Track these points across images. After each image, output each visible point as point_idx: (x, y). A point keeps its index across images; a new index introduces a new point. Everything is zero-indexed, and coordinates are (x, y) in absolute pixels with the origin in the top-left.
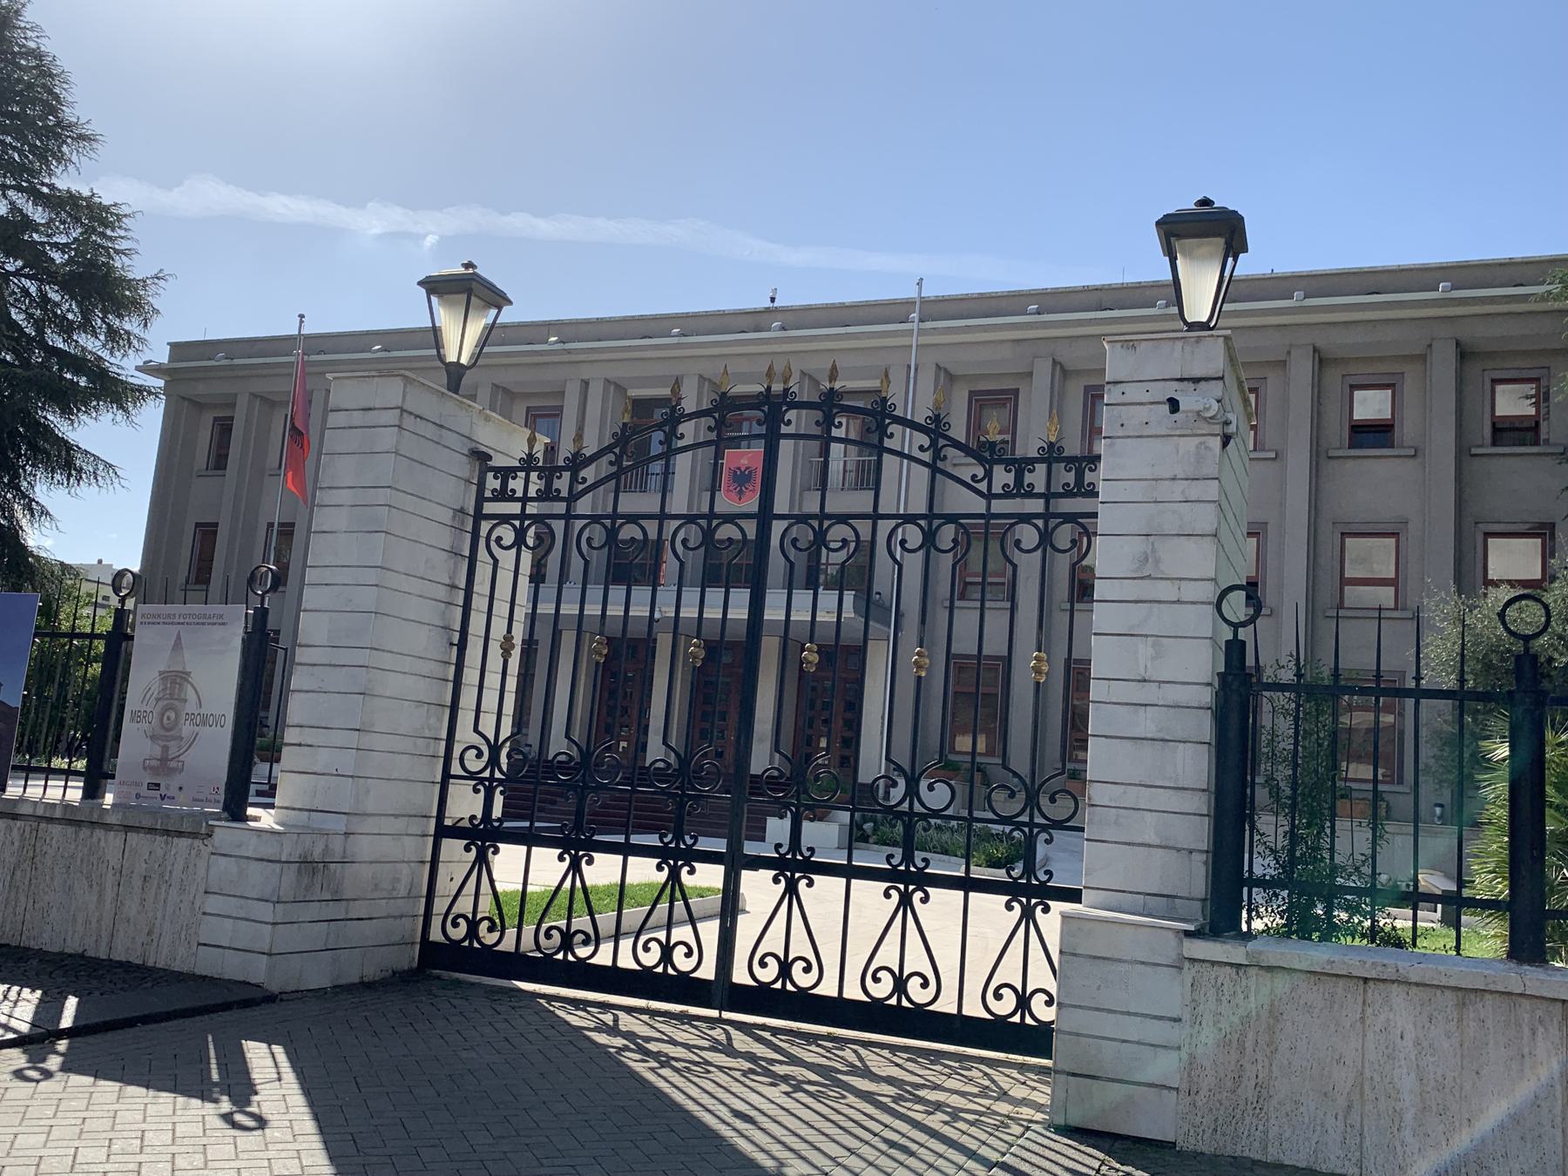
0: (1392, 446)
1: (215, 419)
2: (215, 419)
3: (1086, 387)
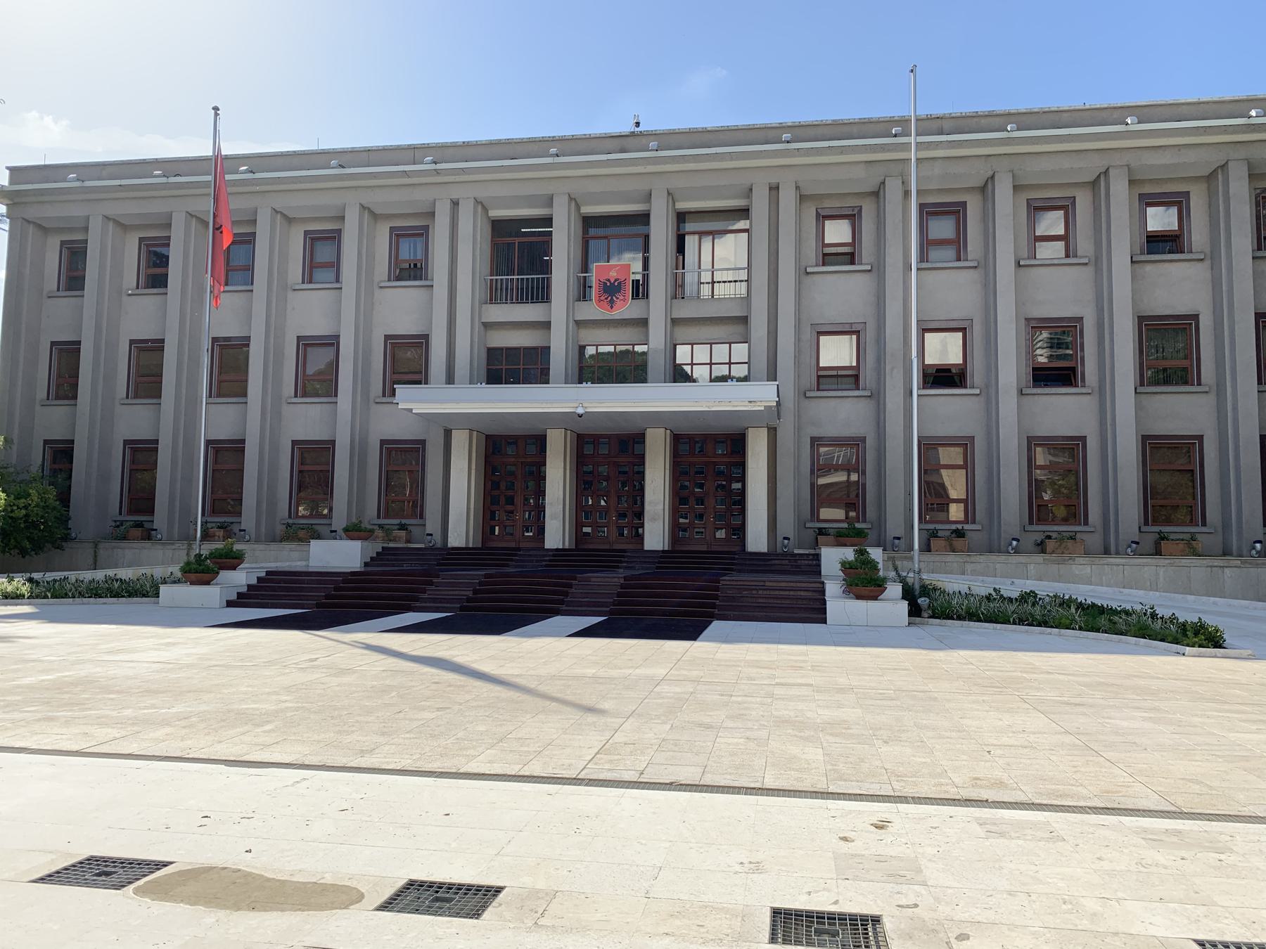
0: (1182, 252)
2: (63, 243)
3: (140, 239)
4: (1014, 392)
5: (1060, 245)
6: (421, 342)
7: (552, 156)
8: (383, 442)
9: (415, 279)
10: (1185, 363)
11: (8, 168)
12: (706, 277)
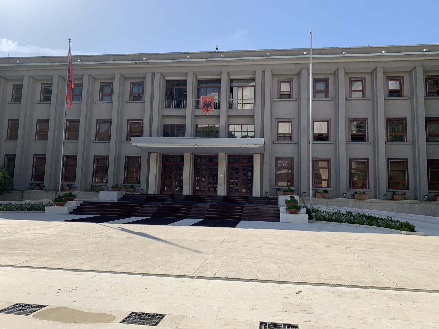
0: (401, 96)
1: (14, 85)
2: (14, 85)
4: (345, 143)
5: (361, 93)
6: (140, 122)
8: (126, 157)
9: (139, 100)
10: (402, 134)
12: (240, 102)
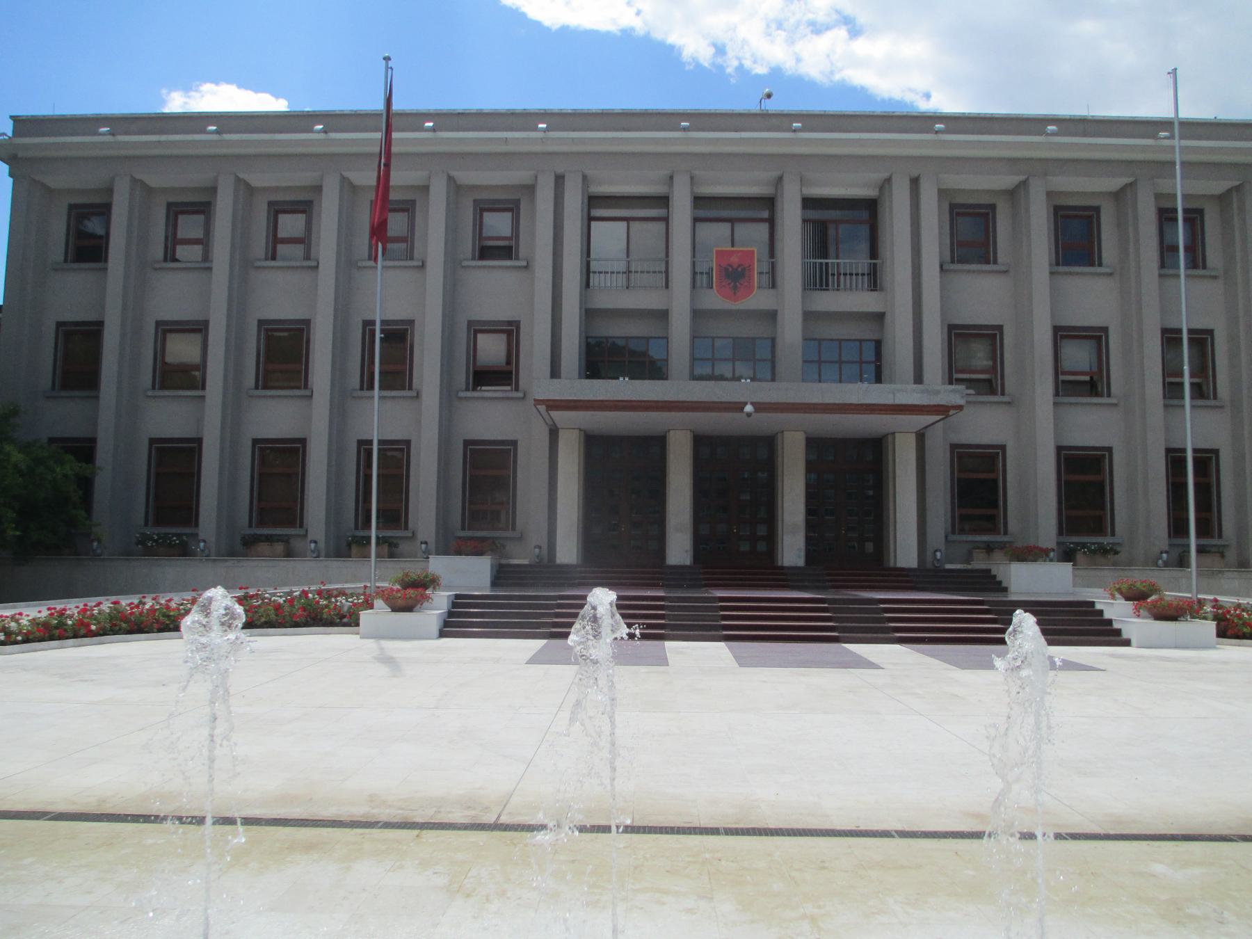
7: (685, 129)
11: (11, 117)
